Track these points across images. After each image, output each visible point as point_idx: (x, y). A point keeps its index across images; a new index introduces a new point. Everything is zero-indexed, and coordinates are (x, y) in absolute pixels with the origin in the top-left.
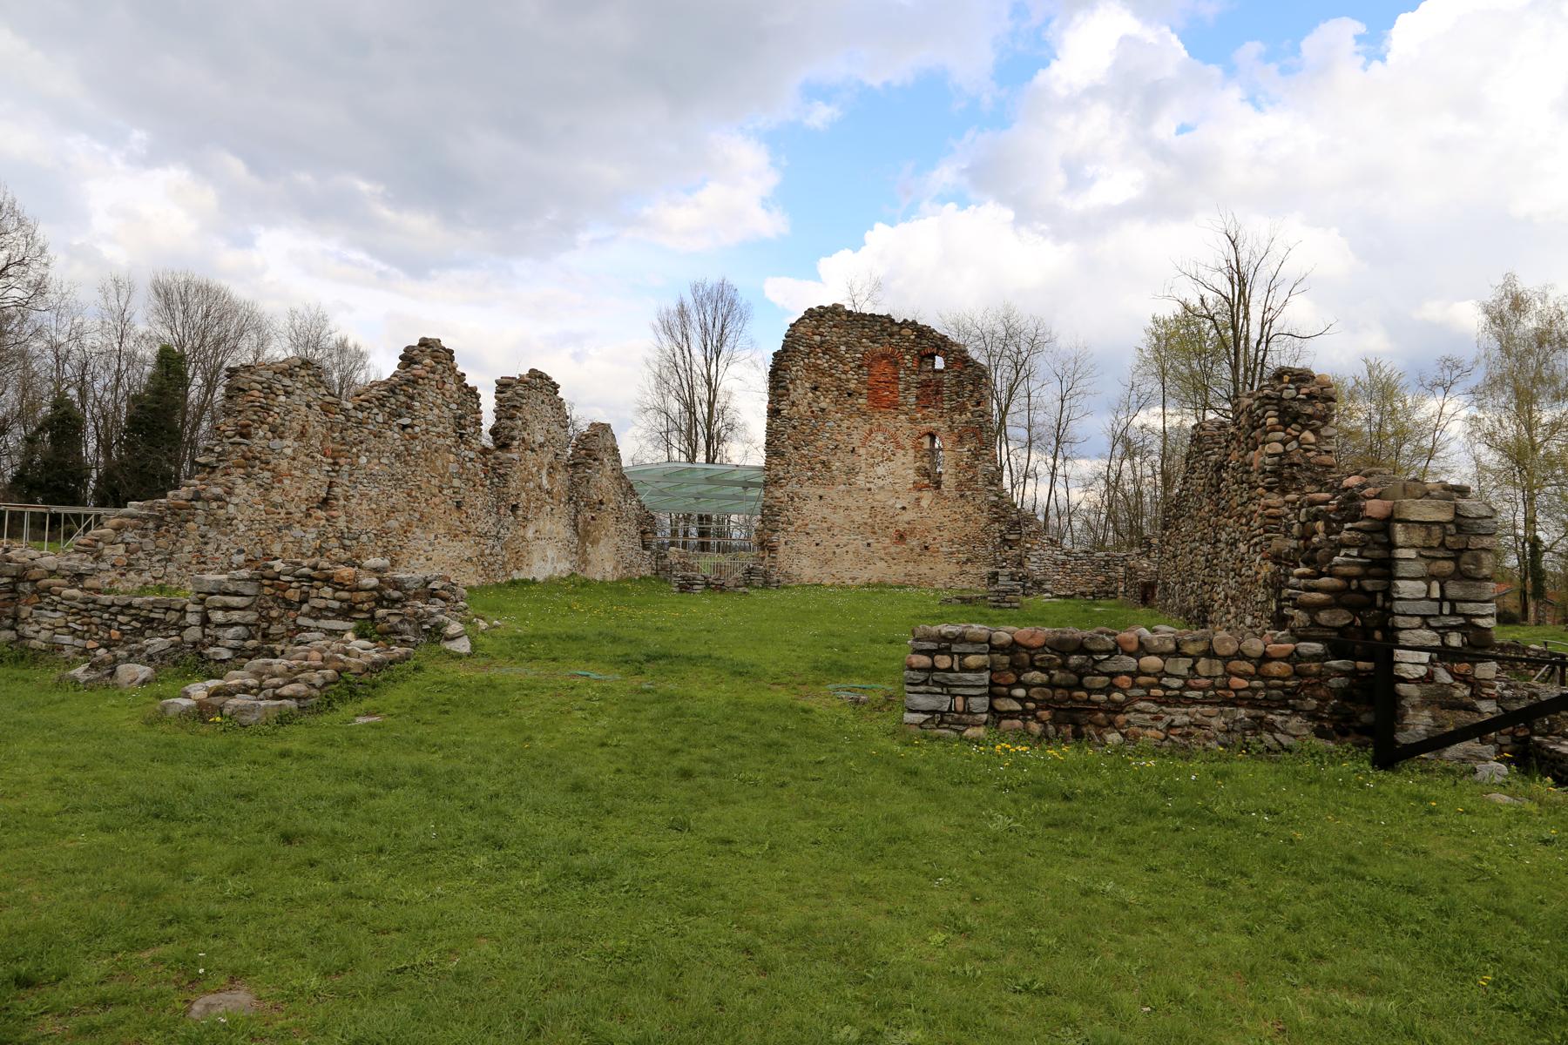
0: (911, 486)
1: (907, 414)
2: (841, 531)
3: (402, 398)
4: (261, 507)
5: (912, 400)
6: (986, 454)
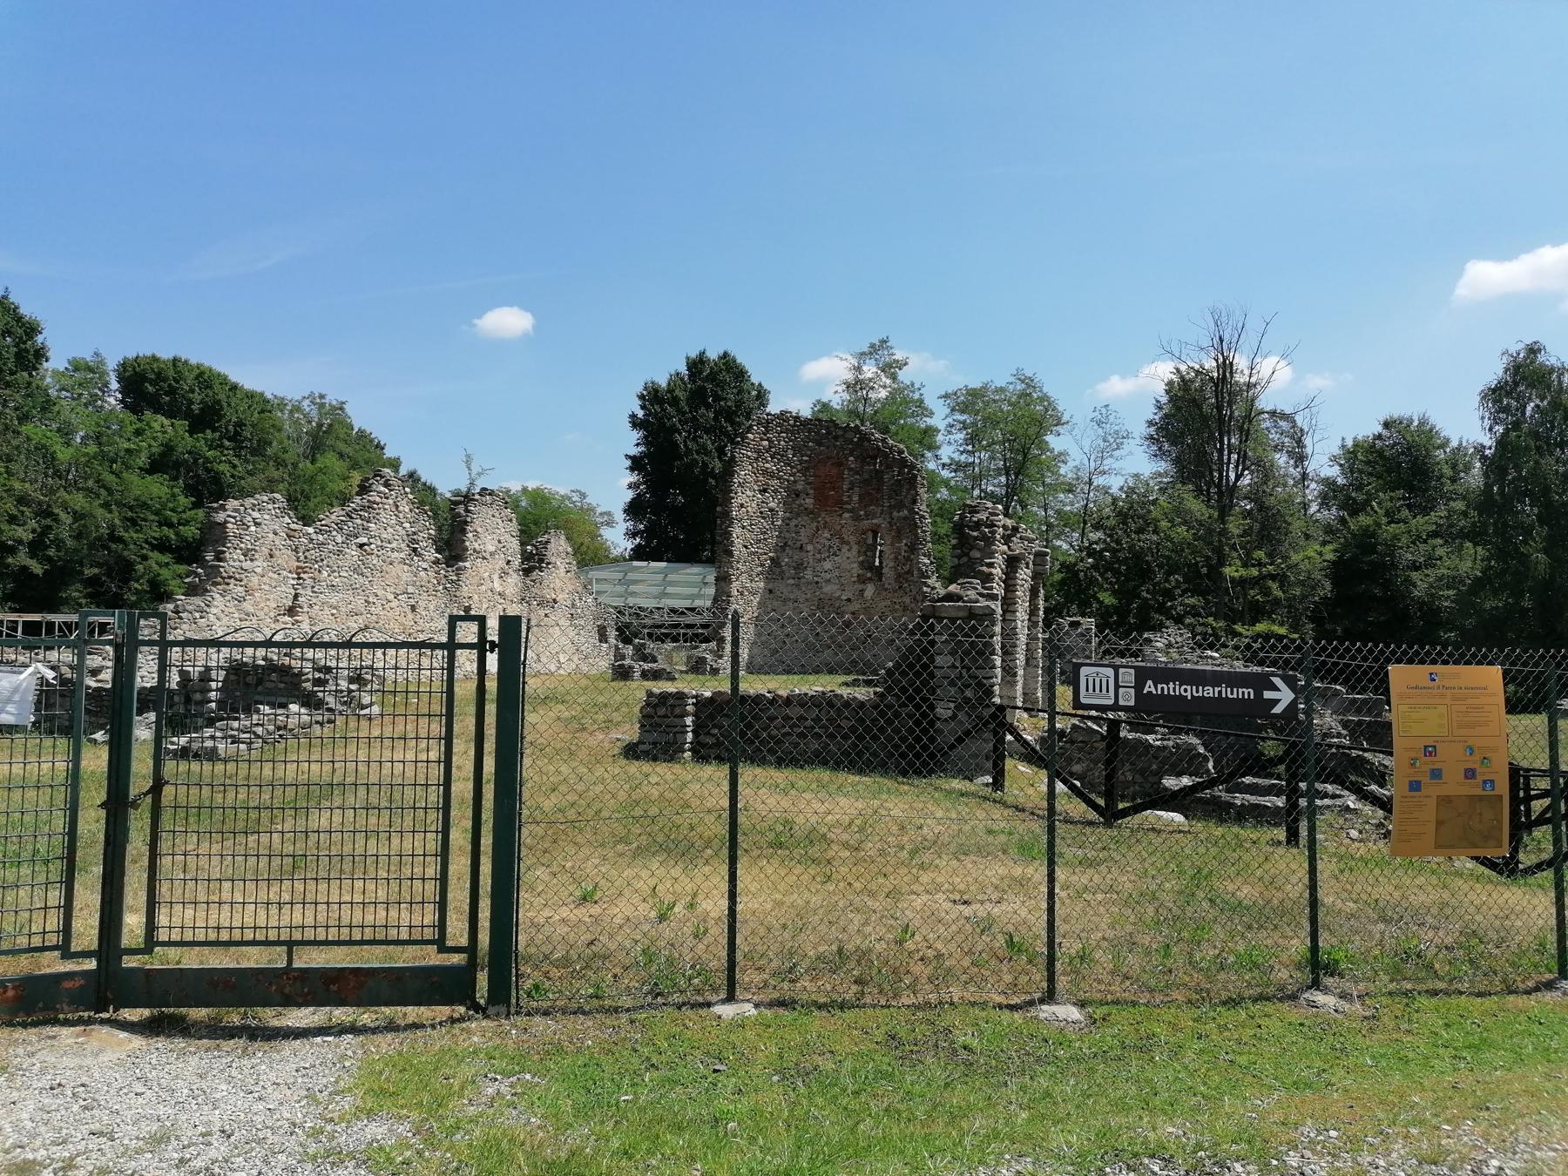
0: (855, 579)
3: (359, 521)
4: (236, 615)
5: (856, 498)
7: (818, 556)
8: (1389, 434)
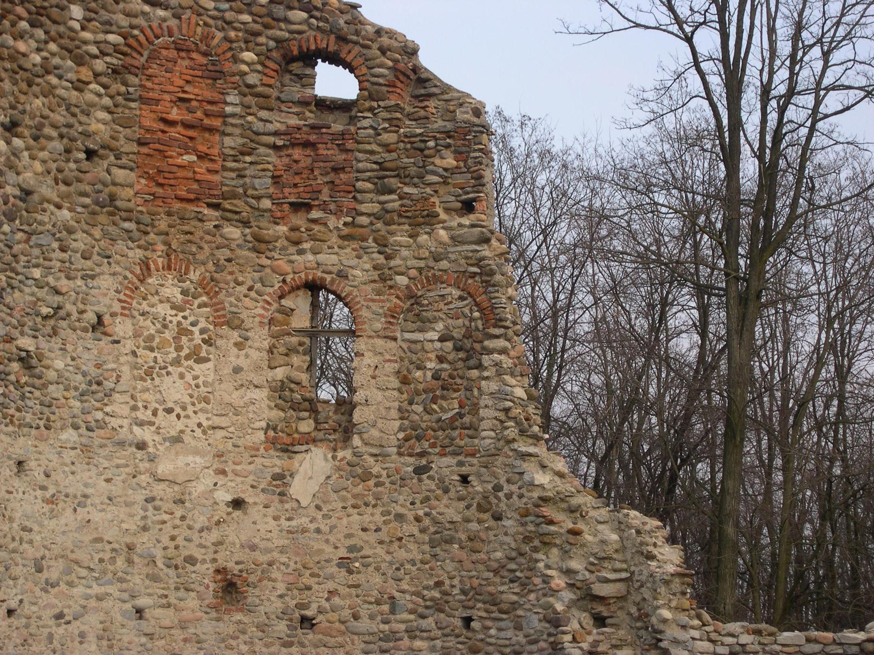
1: (246, 224)
2: (68, 571)
6: (503, 351)
7: (146, 357)
8: (867, 342)
